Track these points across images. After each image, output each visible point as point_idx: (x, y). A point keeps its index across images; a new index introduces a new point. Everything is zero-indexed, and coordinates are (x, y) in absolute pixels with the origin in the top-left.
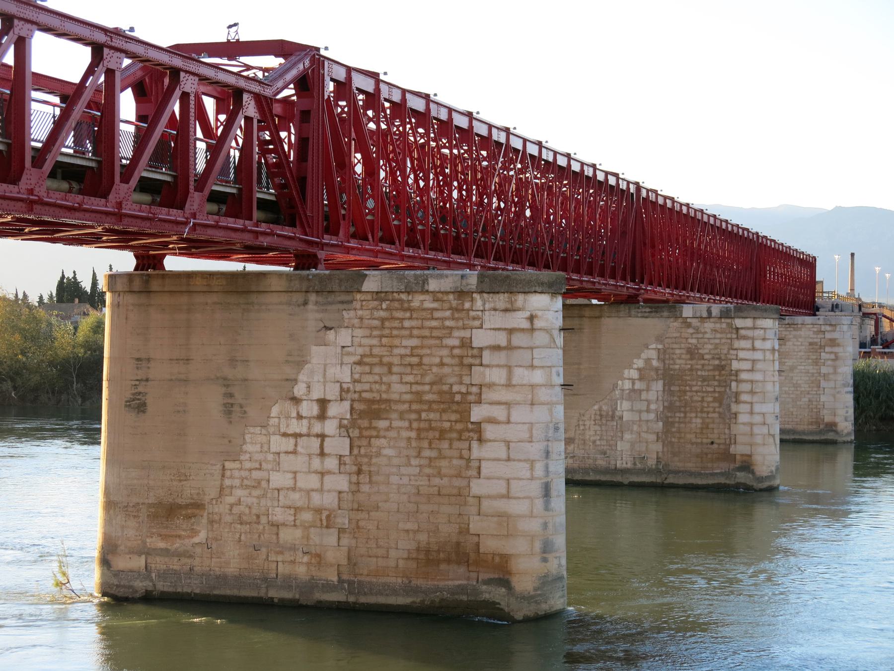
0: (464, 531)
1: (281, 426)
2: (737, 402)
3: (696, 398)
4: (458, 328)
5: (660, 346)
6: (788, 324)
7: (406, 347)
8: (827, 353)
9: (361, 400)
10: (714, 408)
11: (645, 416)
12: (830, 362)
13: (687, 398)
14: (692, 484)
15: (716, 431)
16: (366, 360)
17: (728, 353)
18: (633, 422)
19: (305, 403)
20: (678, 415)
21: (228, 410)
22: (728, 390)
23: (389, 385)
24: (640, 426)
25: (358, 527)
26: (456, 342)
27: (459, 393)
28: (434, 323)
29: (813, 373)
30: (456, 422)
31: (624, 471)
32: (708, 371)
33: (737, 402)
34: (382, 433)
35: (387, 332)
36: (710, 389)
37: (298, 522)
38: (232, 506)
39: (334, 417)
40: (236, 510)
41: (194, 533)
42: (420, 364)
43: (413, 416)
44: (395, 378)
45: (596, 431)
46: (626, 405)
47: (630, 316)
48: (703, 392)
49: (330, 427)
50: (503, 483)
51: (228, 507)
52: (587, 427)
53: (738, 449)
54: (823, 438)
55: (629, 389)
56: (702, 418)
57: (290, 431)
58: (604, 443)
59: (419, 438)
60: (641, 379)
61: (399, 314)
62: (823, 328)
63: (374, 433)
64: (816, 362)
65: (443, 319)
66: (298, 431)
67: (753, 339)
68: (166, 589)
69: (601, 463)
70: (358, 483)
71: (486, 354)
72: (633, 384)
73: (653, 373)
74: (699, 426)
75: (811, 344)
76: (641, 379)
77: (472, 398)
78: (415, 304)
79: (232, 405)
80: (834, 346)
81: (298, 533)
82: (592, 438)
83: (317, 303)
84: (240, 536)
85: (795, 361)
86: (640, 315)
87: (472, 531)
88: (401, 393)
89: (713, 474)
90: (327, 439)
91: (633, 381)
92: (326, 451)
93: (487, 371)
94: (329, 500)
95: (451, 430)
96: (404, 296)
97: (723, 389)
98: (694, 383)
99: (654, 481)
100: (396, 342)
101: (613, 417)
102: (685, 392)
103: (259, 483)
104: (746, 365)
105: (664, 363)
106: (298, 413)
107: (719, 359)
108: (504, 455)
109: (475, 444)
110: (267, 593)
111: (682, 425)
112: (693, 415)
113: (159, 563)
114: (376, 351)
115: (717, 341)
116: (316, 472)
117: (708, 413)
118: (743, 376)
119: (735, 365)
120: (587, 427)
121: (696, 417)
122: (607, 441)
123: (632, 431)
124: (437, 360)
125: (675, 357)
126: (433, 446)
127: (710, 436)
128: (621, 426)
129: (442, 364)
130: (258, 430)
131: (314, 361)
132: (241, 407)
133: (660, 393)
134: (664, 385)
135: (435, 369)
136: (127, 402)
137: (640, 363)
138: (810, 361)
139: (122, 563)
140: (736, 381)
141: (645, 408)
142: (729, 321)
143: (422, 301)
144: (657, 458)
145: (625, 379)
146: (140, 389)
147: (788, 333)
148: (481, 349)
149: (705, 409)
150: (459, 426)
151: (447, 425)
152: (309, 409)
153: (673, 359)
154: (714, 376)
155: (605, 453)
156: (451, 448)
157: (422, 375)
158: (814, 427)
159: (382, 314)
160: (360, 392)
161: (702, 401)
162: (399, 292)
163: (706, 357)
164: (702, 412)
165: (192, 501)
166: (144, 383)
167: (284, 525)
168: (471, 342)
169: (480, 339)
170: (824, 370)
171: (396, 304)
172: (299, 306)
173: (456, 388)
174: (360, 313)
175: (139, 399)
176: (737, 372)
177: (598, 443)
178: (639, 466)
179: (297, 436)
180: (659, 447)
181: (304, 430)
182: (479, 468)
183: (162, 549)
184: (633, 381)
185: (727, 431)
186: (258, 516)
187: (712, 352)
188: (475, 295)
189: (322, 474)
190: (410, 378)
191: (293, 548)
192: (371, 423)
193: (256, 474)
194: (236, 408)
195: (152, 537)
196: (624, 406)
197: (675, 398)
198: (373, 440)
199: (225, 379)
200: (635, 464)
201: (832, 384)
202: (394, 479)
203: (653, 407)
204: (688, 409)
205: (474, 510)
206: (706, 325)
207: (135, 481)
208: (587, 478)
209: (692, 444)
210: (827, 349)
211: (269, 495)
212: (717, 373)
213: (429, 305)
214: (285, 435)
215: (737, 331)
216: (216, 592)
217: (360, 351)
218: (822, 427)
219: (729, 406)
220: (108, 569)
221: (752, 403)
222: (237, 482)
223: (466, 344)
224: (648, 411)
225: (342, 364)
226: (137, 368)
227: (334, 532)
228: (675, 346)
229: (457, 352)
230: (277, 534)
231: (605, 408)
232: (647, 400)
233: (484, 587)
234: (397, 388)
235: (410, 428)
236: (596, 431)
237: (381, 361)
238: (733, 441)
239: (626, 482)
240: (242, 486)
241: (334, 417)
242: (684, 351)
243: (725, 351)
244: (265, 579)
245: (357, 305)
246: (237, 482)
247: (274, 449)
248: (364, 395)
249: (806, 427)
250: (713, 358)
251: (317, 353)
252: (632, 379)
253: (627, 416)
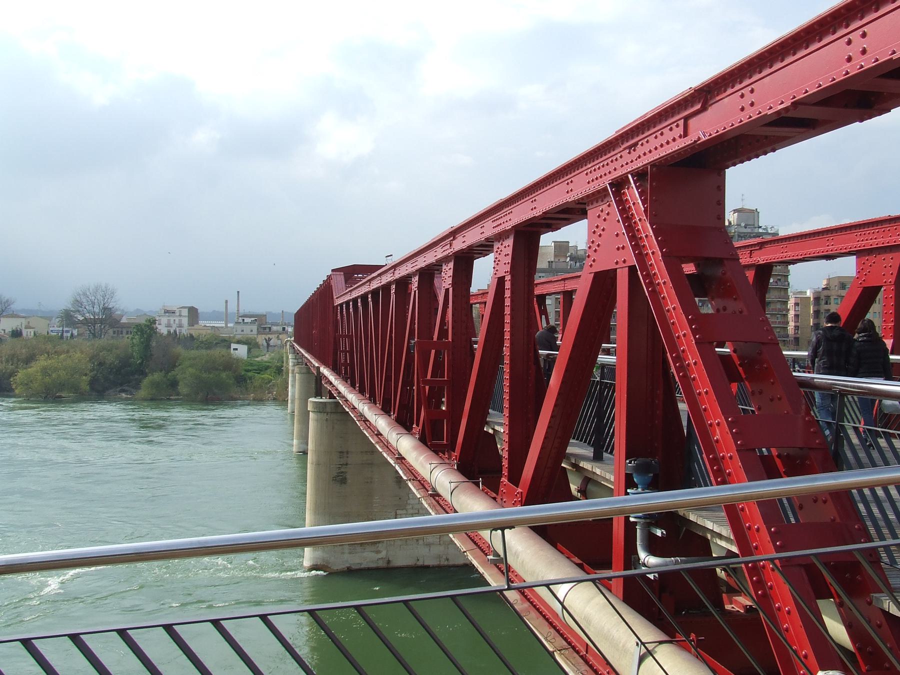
146: (342, 470)
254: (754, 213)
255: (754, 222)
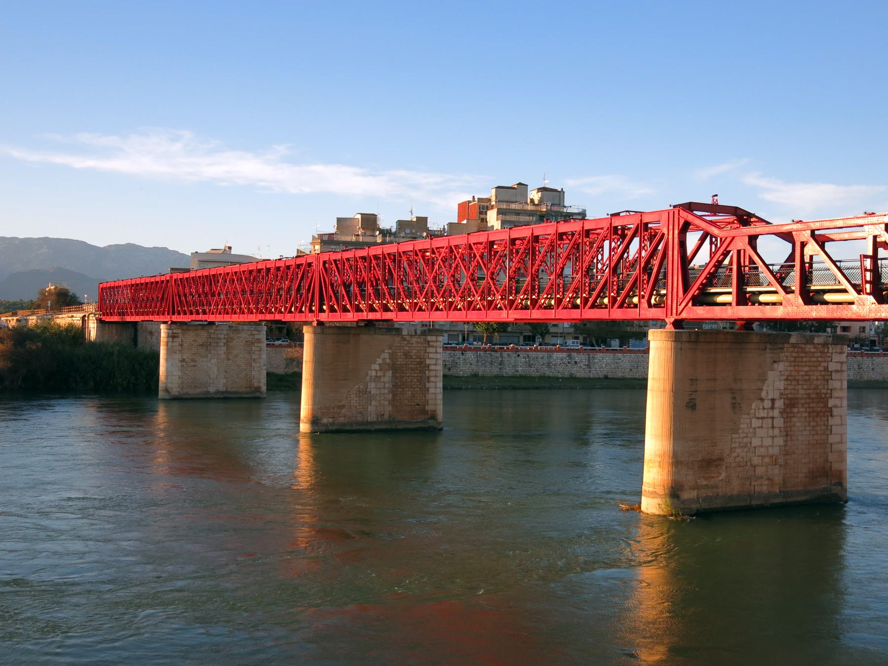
0: (827, 461)
1: (756, 414)
2: (429, 382)
3: (408, 380)
4: (823, 362)
5: (390, 351)
6: (234, 330)
7: (804, 371)
8: (255, 347)
9: (787, 398)
10: (417, 385)
11: (383, 391)
12: (257, 352)
13: (404, 380)
14: (407, 428)
15: (418, 398)
16: (789, 378)
17: (424, 355)
18: (377, 394)
19: (766, 401)
20: (399, 390)
21: (734, 406)
22: (424, 375)
23: (798, 390)
24: (380, 397)
25: (787, 463)
26: (822, 369)
27: (823, 393)
28: (814, 359)
29: (248, 359)
30: (822, 407)
31: (372, 423)
32: (415, 364)
33: (429, 382)
34: (796, 415)
35: (797, 363)
36: (416, 375)
37: (763, 464)
38: (735, 458)
39: (777, 408)
40: (737, 460)
41: (720, 474)
42: (809, 380)
43: (807, 406)
44: (800, 387)
45: (356, 401)
46: (373, 385)
47: (376, 334)
48: (412, 377)
49: (776, 413)
50: (840, 436)
51: (733, 458)
52: (352, 398)
53: (429, 408)
54: (253, 396)
55: (374, 376)
56: (412, 391)
57: (760, 416)
58: (361, 407)
59: (809, 416)
60: (380, 370)
61: (801, 355)
62: (253, 333)
63: (792, 415)
64: (250, 352)
65: (817, 357)
66: (763, 416)
67: (436, 347)
68: (706, 507)
69: (360, 419)
70: (786, 441)
71: (833, 374)
72: (377, 373)
73: (387, 367)
74: (410, 395)
75: (246, 341)
76: (380, 370)
77: (828, 396)
78: (807, 350)
79: (735, 403)
80: (259, 343)
81: (764, 468)
82: (355, 405)
83: (770, 349)
84: (739, 473)
85: (238, 351)
86: (381, 333)
87: (829, 461)
88: (802, 394)
89: (417, 422)
90: (775, 419)
91: (376, 371)
92: (775, 425)
93: (834, 382)
94: (775, 451)
95: (821, 411)
96: (803, 346)
97: (421, 375)
98: (407, 372)
99: (388, 427)
100: (800, 368)
101: (366, 392)
102: (403, 376)
103: (747, 445)
104: (433, 362)
105: (392, 361)
106: (763, 407)
107: (420, 358)
108: (840, 423)
109: (830, 418)
110: (750, 503)
111: (401, 396)
112: (407, 389)
113: (703, 493)
114: (793, 373)
115: (419, 348)
116: (771, 437)
117: (414, 388)
118: (432, 367)
119: (428, 362)
120: (352, 398)
121: (409, 391)
122: (363, 406)
123: (376, 399)
124: (815, 378)
125: (397, 357)
126: (815, 420)
127: (416, 401)
128: (370, 397)
129: (817, 380)
130: (746, 416)
131: (770, 379)
132: (739, 404)
133: (391, 378)
134: (393, 373)
135: (815, 382)
136: (686, 404)
137: (380, 361)
138: (246, 351)
139: (686, 495)
140: (428, 370)
141: (383, 386)
142: (424, 337)
143: (810, 348)
144: (389, 414)
145: (372, 370)
146: (693, 397)
147: (233, 335)
148: (831, 372)
149: (413, 386)
150: (824, 410)
151: (819, 409)
152: (767, 404)
153: (397, 358)
154: (417, 368)
155: (362, 413)
156: (821, 420)
157: (810, 385)
158: (249, 389)
159: (795, 354)
160: (787, 394)
161: (412, 382)
162: (801, 344)
163: (413, 357)
164: (411, 388)
165: (718, 457)
166: (694, 393)
167: (758, 465)
168: (828, 368)
169: (832, 367)
170: (254, 357)
171: (800, 350)
172: (763, 350)
173: (822, 391)
174: (786, 354)
175: (692, 402)
176: (429, 365)
177: (358, 407)
178: (380, 419)
179: (763, 418)
180: (390, 408)
181: (765, 415)
182: (831, 430)
183: (705, 485)
184: (376, 371)
185: (424, 398)
186: (746, 462)
187: (416, 354)
188: (829, 345)
189: (773, 437)
190: (805, 387)
191: (761, 478)
192: (791, 410)
193: (745, 440)
194: (737, 405)
195: (700, 479)
196: (372, 385)
197: (398, 381)
198: (792, 418)
199: (732, 389)
200: (378, 419)
201: (258, 365)
202: (800, 438)
203: (387, 385)
204: (404, 386)
205: (829, 450)
206: (413, 339)
207: (692, 449)
208: (353, 428)
209: (407, 405)
210: (256, 345)
211: (751, 450)
212: (419, 366)
213: (812, 350)
214: (758, 418)
215: (428, 343)
216: (728, 505)
217: (787, 373)
218: (253, 389)
219: (425, 384)
220: (678, 500)
221: (436, 382)
222: (737, 445)
223: (826, 369)
224: (384, 388)
225: (780, 380)
226: (692, 385)
227: (778, 466)
228: (398, 351)
229: (823, 373)
230: (755, 471)
231: (361, 387)
232: (384, 382)
233: (833, 487)
234: (801, 392)
235: (806, 412)
236: (356, 401)
237: (795, 378)
238: (427, 403)
239: (373, 429)
240: (741, 447)
241: (777, 408)
242: (402, 354)
243: (423, 354)
244: (750, 495)
245: (785, 350)
246: (737, 445)
247: (753, 426)
248: (789, 396)
249: (244, 390)
250: (417, 358)
251: (771, 375)
252: (376, 370)
253: (373, 391)
254: (560, 194)
255: (560, 202)
